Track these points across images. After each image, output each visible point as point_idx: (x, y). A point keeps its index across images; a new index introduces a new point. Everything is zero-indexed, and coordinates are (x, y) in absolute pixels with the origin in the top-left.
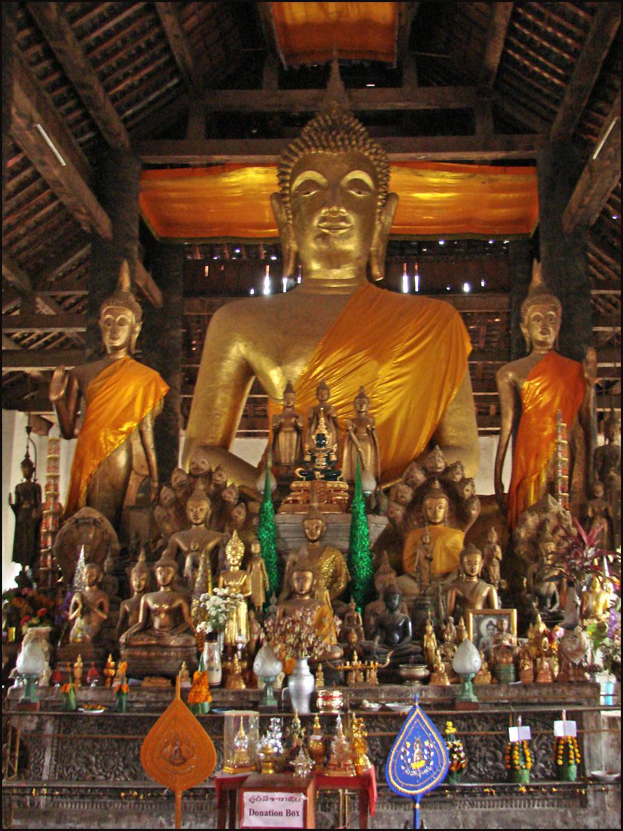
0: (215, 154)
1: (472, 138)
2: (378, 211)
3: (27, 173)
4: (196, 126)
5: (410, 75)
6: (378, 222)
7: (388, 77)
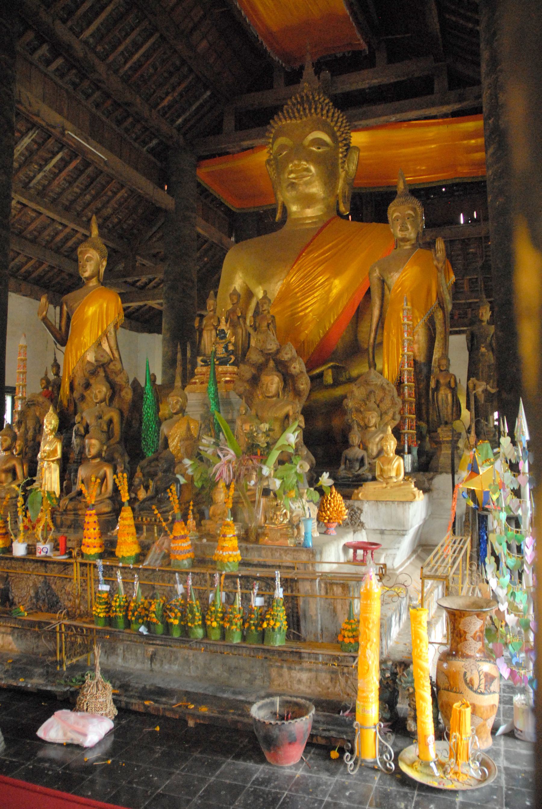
0: (244, 140)
1: (433, 97)
2: (340, 161)
3: (90, 170)
4: (229, 123)
5: (381, 57)
6: (341, 170)
7: (354, 62)
